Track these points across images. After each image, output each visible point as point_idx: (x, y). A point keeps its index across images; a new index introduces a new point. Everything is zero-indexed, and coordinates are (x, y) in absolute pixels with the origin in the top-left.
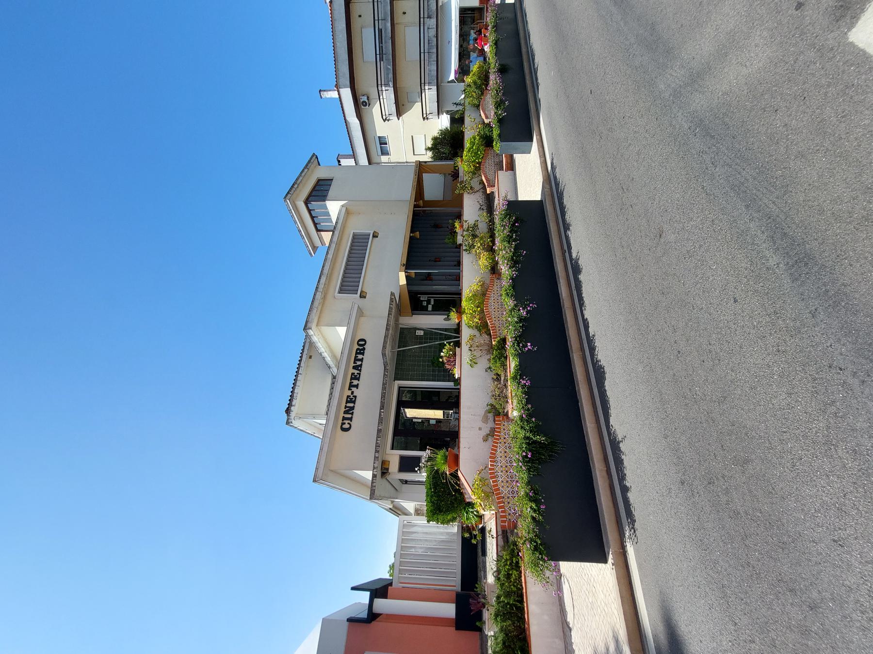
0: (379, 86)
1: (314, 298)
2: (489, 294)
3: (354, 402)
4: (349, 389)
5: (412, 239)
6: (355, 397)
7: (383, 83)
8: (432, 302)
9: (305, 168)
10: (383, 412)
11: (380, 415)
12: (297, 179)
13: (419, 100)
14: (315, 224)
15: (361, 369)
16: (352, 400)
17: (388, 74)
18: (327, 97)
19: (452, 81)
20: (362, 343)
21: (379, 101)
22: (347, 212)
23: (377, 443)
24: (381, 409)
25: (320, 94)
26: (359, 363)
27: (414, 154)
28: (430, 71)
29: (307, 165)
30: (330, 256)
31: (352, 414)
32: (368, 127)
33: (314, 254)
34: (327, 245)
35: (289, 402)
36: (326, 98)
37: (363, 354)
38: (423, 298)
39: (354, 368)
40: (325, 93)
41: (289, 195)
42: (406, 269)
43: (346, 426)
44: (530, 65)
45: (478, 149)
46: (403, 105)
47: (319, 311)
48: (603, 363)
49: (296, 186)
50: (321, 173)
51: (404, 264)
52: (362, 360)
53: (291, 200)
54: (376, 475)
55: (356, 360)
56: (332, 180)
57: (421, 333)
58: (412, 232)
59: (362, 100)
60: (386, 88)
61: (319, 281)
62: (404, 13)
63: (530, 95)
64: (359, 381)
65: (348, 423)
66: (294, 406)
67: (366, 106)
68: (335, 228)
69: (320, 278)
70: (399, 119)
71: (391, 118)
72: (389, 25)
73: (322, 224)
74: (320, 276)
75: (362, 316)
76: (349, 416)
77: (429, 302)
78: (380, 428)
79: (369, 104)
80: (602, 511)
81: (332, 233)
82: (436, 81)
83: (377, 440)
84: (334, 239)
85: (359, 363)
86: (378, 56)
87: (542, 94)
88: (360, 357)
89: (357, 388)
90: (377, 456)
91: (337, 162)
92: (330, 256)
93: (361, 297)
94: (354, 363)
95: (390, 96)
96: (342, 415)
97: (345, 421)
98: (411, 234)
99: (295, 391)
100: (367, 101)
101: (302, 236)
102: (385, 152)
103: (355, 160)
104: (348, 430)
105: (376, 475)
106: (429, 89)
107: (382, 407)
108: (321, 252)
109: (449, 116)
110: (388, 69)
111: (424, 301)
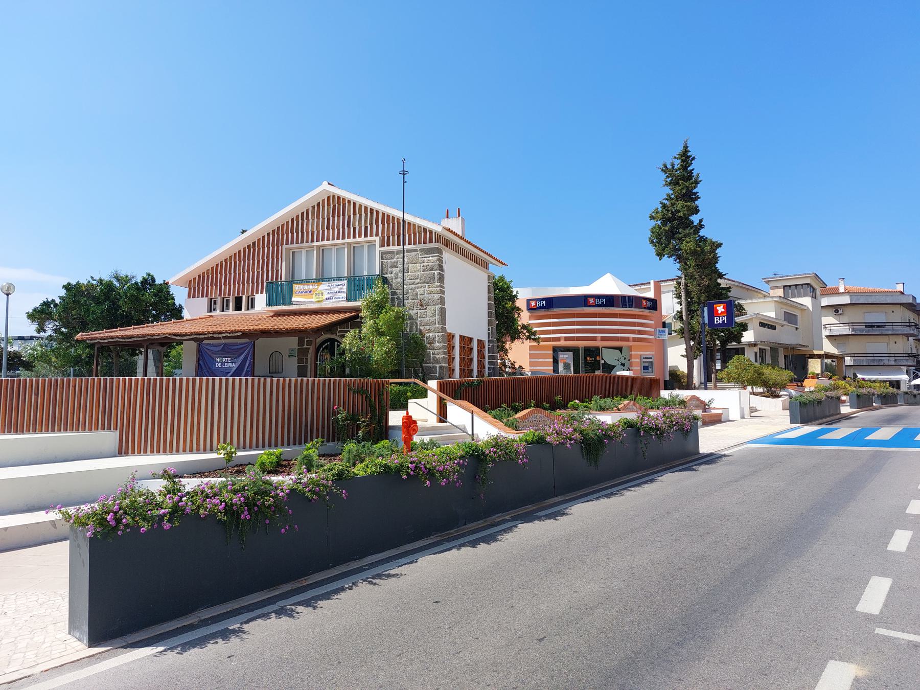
0: (852, 324)
7: (854, 327)
17: (860, 331)
21: (839, 323)
40: (843, 282)
60: (851, 329)
61: (752, 287)
62: (895, 343)
67: (835, 312)
68: (786, 299)
72: (890, 333)
73: (790, 291)
81: (783, 296)
86: (871, 324)
95: (845, 331)
110: (863, 331)
111: (816, 376)
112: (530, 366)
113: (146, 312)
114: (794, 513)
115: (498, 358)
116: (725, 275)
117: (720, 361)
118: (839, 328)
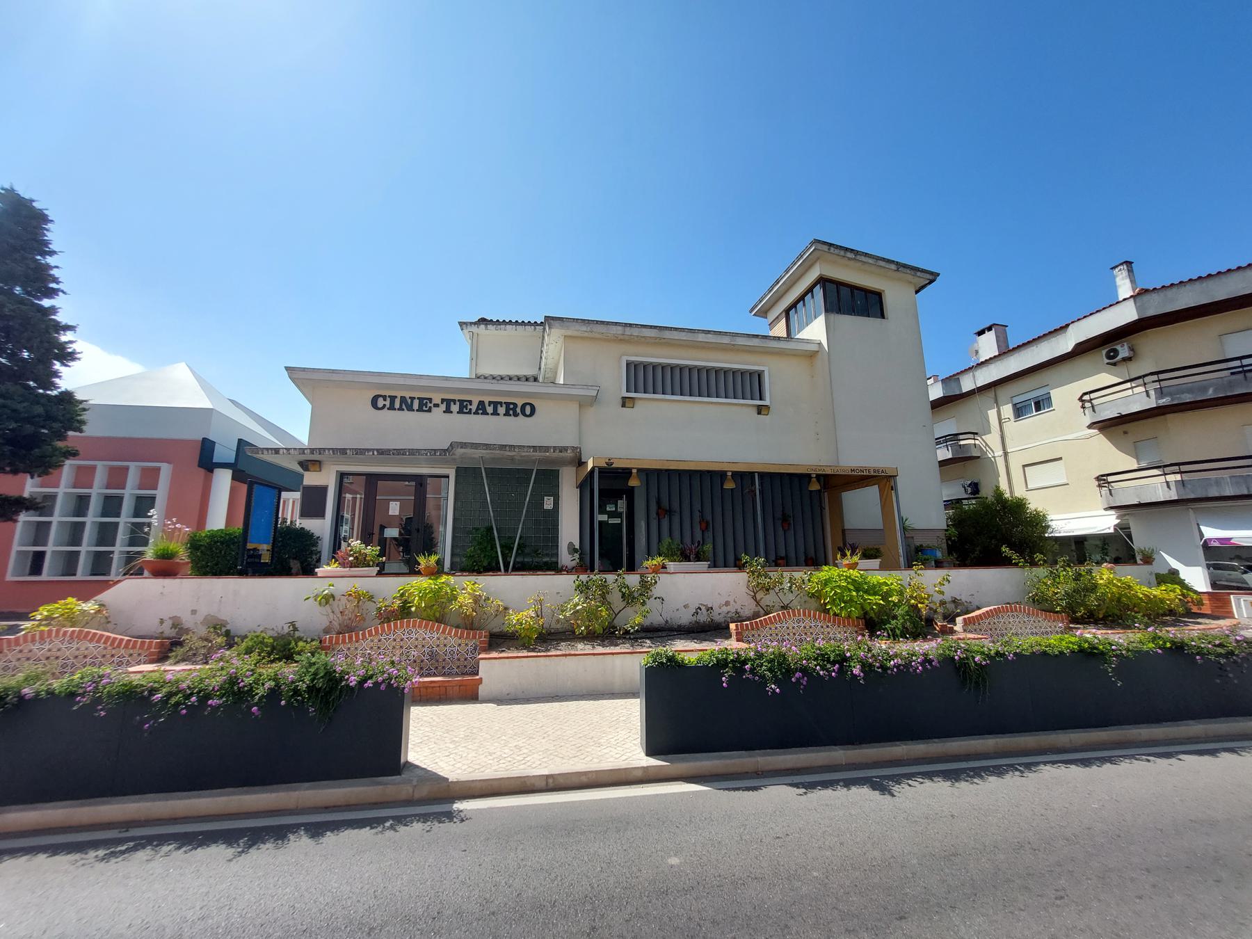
0: (1155, 378)
1: (608, 323)
2: (438, 629)
3: (420, 410)
4: (443, 401)
5: (722, 475)
6: (429, 410)
7: (1164, 384)
8: (612, 521)
9: (897, 264)
10: (373, 454)
11: (368, 450)
12: (866, 255)
13: (1143, 465)
14: (794, 306)
15: (478, 414)
16: (425, 405)
17: (1190, 391)
18: (1117, 279)
19: (1202, 535)
20: (528, 410)
21: (1122, 380)
22: (811, 355)
23: (324, 449)
24: (377, 450)
25: (1122, 264)
26: (490, 409)
27: (1024, 466)
28: (1218, 482)
29: (905, 266)
30: (701, 337)
31: (401, 409)
32: (1064, 369)
33: (754, 315)
34: (771, 334)
35: (520, 321)
36: (1114, 277)
37: (507, 414)
38: (622, 505)
39: (481, 403)
40: (1125, 273)
41: (825, 248)
42: (600, 468)
43: (381, 403)
44: (1076, 750)
45: (851, 601)
46: (1125, 433)
47: (586, 334)
48: (1008, 777)
49: (850, 255)
50: (895, 294)
51: (612, 464)
52: (495, 413)
53: (817, 252)
54: (279, 454)
55: (495, 404)
56: (883, 316)
57: (548, 504)
58: (735, 474)
59: (1118, 347)
60: (1152, 393)
63: (838, 754)
64: (504, 415)
65: (385, 405)
66: (486, 329)
67: (1109, 357)
69: (651, 327)
70: (1090, 427)
71: (1086, 411)
74: (655, 327)
75: (580, 406)
76: (397, 405)
77: (612, 515)
78: (348, 451)
79: (1114, 364)
80: (697, 760)
82: (1192, 496)
83: (329, 449)
84: (741, 339)
85: (490, 409)
86: (1237, 363)
87: (779, 795)
88: (502, 410)
89: (444, 412)
90: (306, 452)
91: (988, 325)
92: (701, 337)
93: (624, 398)
94: (489, 402)
96: (399, 394)
97: (388, 399)
98: (730, 474)
99: (508, 326)
100: (1119, 357)
101: (772, 287)
102: (1019, 412)
103: (995, 357)
104: (375, 408)
105: (279, 454)
106: (1167, 483)
107: (381, 452)
108: (759, 326)
109: (1112, 531)
112: (1206, 561)
113: (753, 491)
114: (506, 751)
115: (614, 509)
116: (79, 353)
117: (215, 460)
118: (1130, 392)
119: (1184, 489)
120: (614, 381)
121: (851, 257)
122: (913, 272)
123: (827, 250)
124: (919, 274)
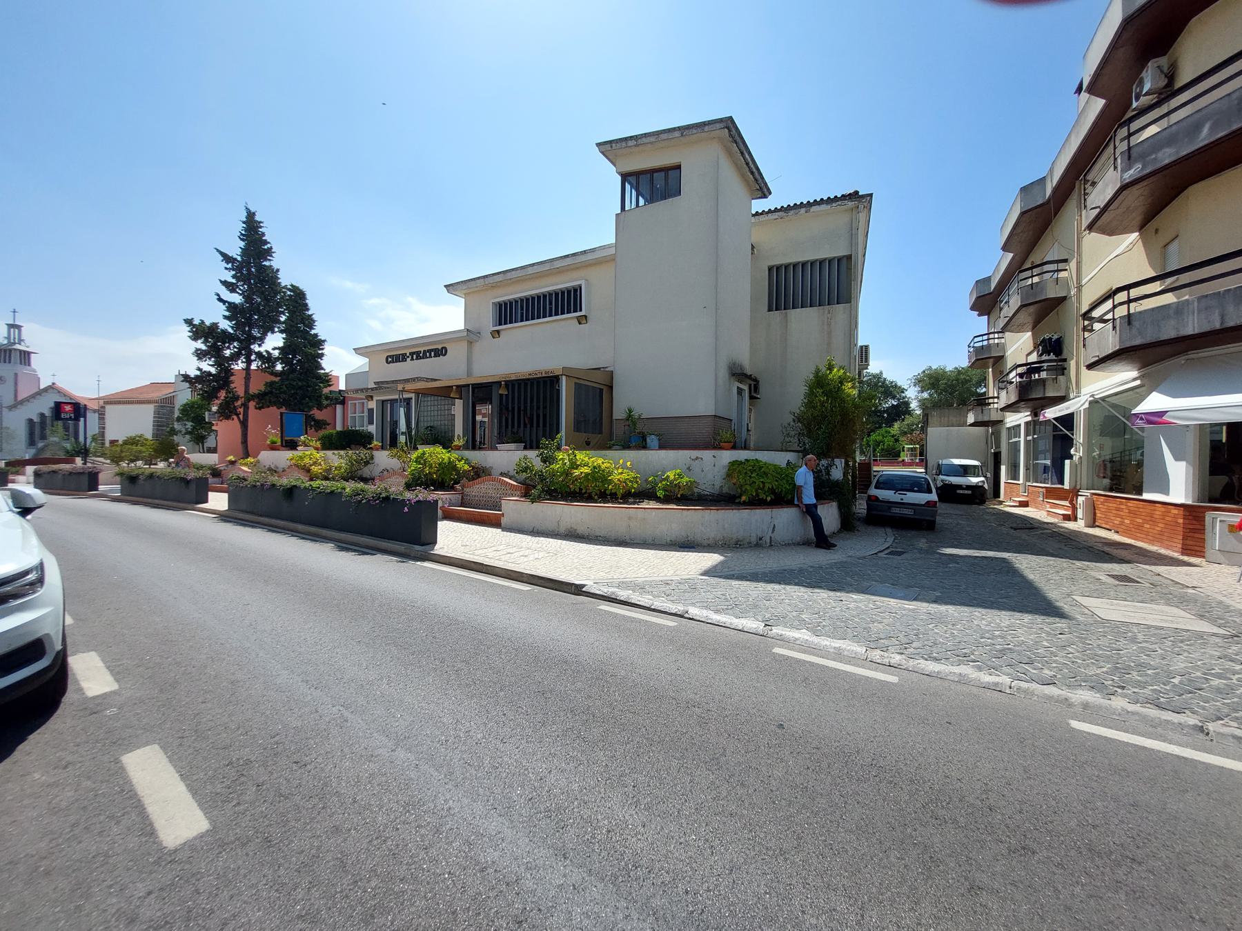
9: (679, 128)
43: (390, 359)
92: (530, 270)
119: (1130, 329)
120: (487, 319)
121: (632, 144)
122: (699, 130)
123: (610, 149)
124: (706, 128)
